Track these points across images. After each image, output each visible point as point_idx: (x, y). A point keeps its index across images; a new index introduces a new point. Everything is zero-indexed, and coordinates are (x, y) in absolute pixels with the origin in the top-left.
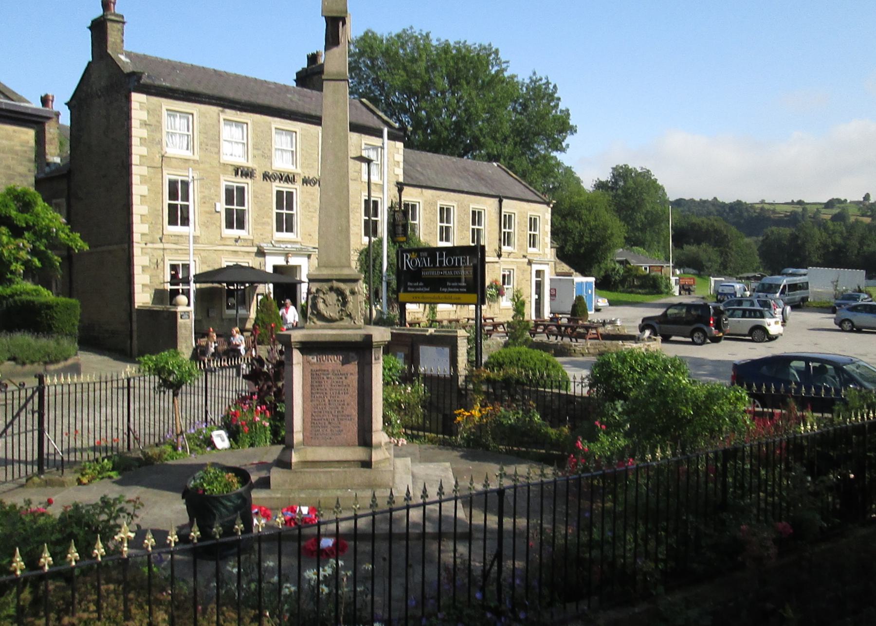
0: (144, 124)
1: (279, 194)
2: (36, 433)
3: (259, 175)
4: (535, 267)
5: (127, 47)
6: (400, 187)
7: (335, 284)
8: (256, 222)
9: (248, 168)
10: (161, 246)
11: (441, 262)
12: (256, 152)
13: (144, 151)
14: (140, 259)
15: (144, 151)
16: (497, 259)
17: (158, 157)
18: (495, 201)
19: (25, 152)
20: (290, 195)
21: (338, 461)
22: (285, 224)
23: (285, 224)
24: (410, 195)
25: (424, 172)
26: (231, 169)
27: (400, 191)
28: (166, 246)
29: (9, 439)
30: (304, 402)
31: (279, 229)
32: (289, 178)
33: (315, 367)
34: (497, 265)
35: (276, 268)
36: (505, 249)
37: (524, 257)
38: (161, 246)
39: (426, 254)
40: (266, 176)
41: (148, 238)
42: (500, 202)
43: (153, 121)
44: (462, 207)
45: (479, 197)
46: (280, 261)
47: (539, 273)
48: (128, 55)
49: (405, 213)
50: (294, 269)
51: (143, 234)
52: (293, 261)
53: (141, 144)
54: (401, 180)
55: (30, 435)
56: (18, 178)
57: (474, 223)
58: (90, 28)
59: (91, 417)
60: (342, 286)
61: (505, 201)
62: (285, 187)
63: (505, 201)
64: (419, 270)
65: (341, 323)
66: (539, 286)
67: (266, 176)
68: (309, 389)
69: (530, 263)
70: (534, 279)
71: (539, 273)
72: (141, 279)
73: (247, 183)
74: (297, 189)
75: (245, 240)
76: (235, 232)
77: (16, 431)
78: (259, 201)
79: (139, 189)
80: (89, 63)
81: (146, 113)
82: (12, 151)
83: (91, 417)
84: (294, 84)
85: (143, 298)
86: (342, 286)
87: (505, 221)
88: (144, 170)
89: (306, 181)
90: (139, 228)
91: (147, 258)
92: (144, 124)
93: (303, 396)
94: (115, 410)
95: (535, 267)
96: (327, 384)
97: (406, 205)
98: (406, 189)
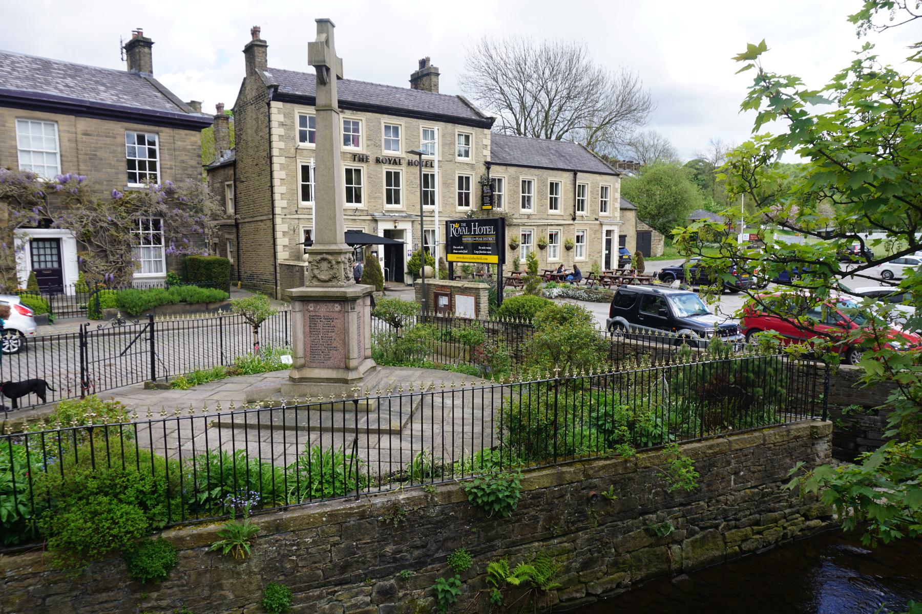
0: (282, 124)
1: (389, 174)
2: (149, 354)
3: (372, 159)
4: (605, 228)
5: (270, 65)
6: (488, 165)
7: (325, 256)
8: (370, 197)
9: (363, 155)
10: (297, 216)
11: (475, 231)
12: (369, 143)
13: (282, 145)
14: (281, 227)
15: (282, 145)
16: (571, 222)
17: (293, 150)
18: (571, 175)
19: (195, 150)
20: (397, 175)
21: (327, 379)
22: (393, 197)
23: (393, 197)
24: (496, 172)
25: (511, 153)
26: (349, 156)
27: (488, 168)
28: (301, 216)
29: (128, 357)
30: (305, 337)
31: (389, 201)
32: (396, 162)
33: (312, 314)
34: (572, 227)
35: (387, 232)
36: (578, 213)
37: (597, 219)
38: (297, 216)
39: (464, 225)
40: (378, 161)
41: (286, 211)
42: (575, 174)
43: (289, 122)
44: (542, 182)
45: (560, 172)
46: (390, 226)
47: (609, 233)
48: (271, 70)
49: (492, 188)
50: (400, 233)
51: (283, 208)
52: (400, 226)
53: (280, 140)
54: (489, 159)
55: (144, 354)
56: (190, 169)
57: (551, 193)
58: (244, 51)
59: (191, 341)
60: (330, 257)
61: (579, 174)
62: (393, 169)
63: (579, 174)
64: (461, 236)
65: (330, 284)
66: (609, 242)
67: (378, 161)
68: (308, 329)
69: (601, 224)
70: (604, 238)
71: (609, 233)
72: (281, 241)
73: (364, 168)
74: (364, 168)
75: (362, 211)
76: (354, 205)
77: (133, 352)
78: (372, 181)
79: (279, 174)
80: (245, 79)
81: (282, 116)
82: (185, 149)
83: (191, 341)
84: (408, 86)
85: (283, 256)
86: (330, 257)
87: (579, 190)
88: (283, 160)
89: (410, 163)
90: (280, 204)
91: (286, 225)
92: (282, 124)
93: (304, 333)
94: (244, 337)
95: (605, 228)
96: (320, 325)
97: (494, 180)
98: (493, 167)
